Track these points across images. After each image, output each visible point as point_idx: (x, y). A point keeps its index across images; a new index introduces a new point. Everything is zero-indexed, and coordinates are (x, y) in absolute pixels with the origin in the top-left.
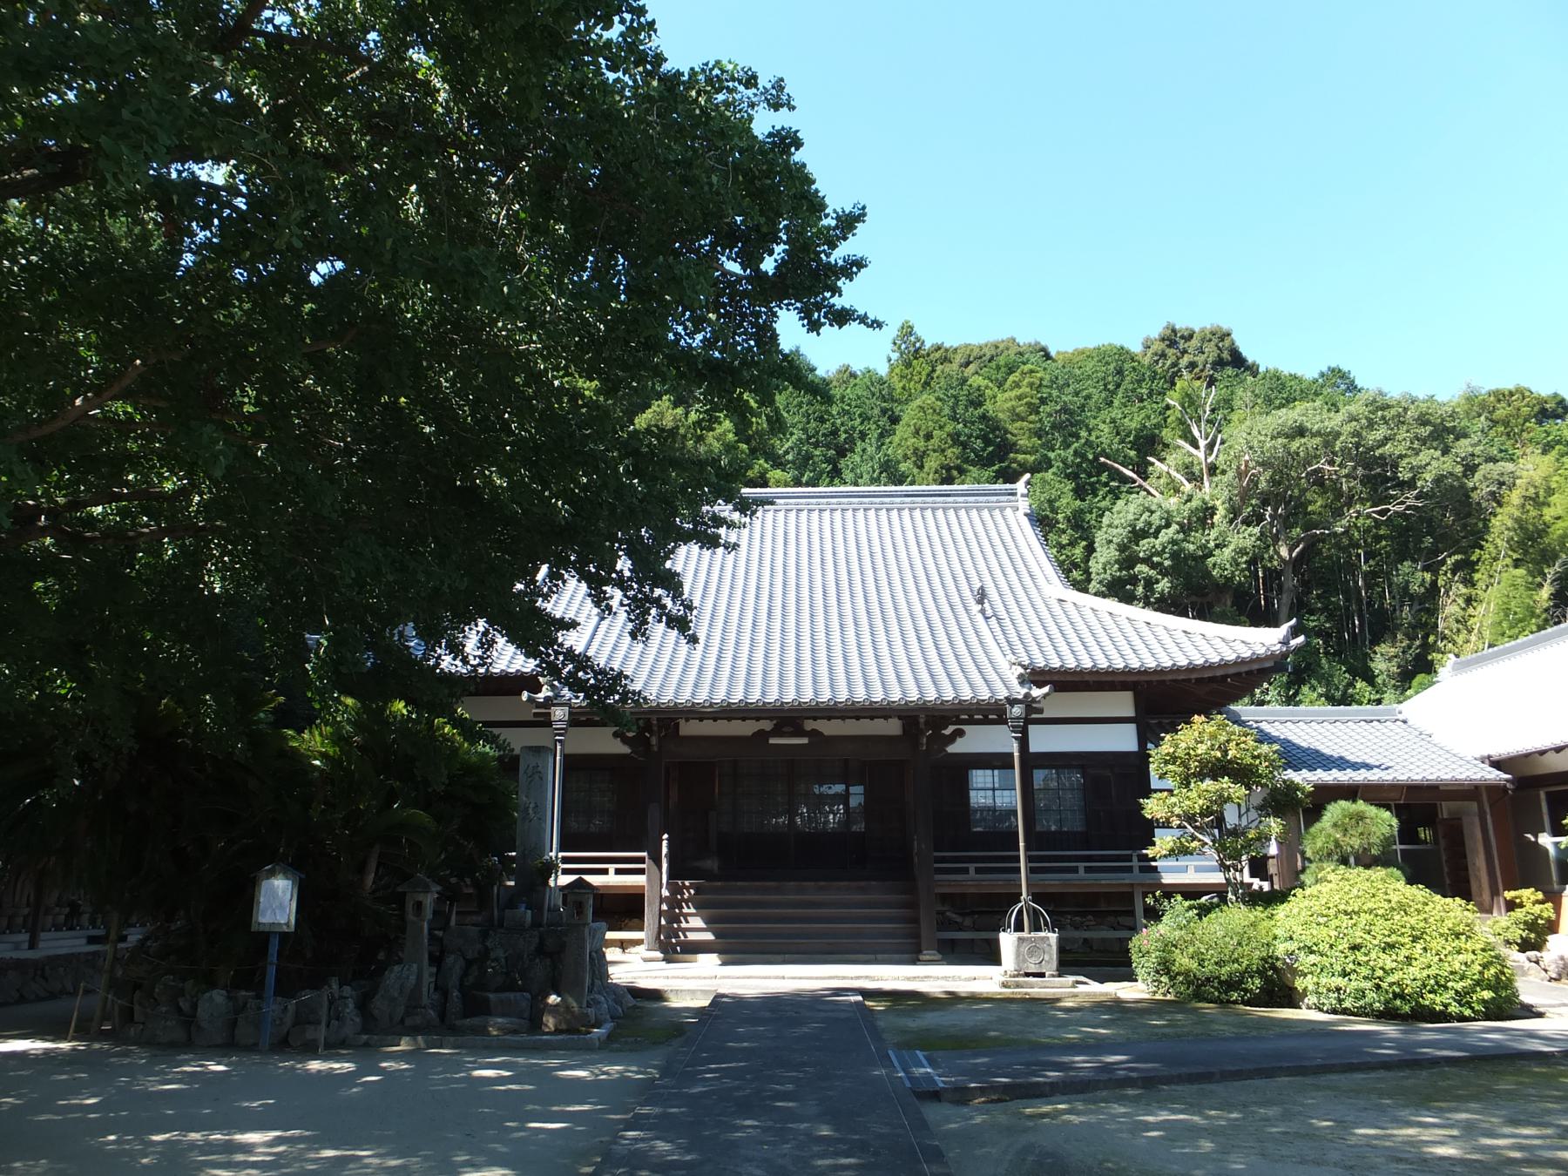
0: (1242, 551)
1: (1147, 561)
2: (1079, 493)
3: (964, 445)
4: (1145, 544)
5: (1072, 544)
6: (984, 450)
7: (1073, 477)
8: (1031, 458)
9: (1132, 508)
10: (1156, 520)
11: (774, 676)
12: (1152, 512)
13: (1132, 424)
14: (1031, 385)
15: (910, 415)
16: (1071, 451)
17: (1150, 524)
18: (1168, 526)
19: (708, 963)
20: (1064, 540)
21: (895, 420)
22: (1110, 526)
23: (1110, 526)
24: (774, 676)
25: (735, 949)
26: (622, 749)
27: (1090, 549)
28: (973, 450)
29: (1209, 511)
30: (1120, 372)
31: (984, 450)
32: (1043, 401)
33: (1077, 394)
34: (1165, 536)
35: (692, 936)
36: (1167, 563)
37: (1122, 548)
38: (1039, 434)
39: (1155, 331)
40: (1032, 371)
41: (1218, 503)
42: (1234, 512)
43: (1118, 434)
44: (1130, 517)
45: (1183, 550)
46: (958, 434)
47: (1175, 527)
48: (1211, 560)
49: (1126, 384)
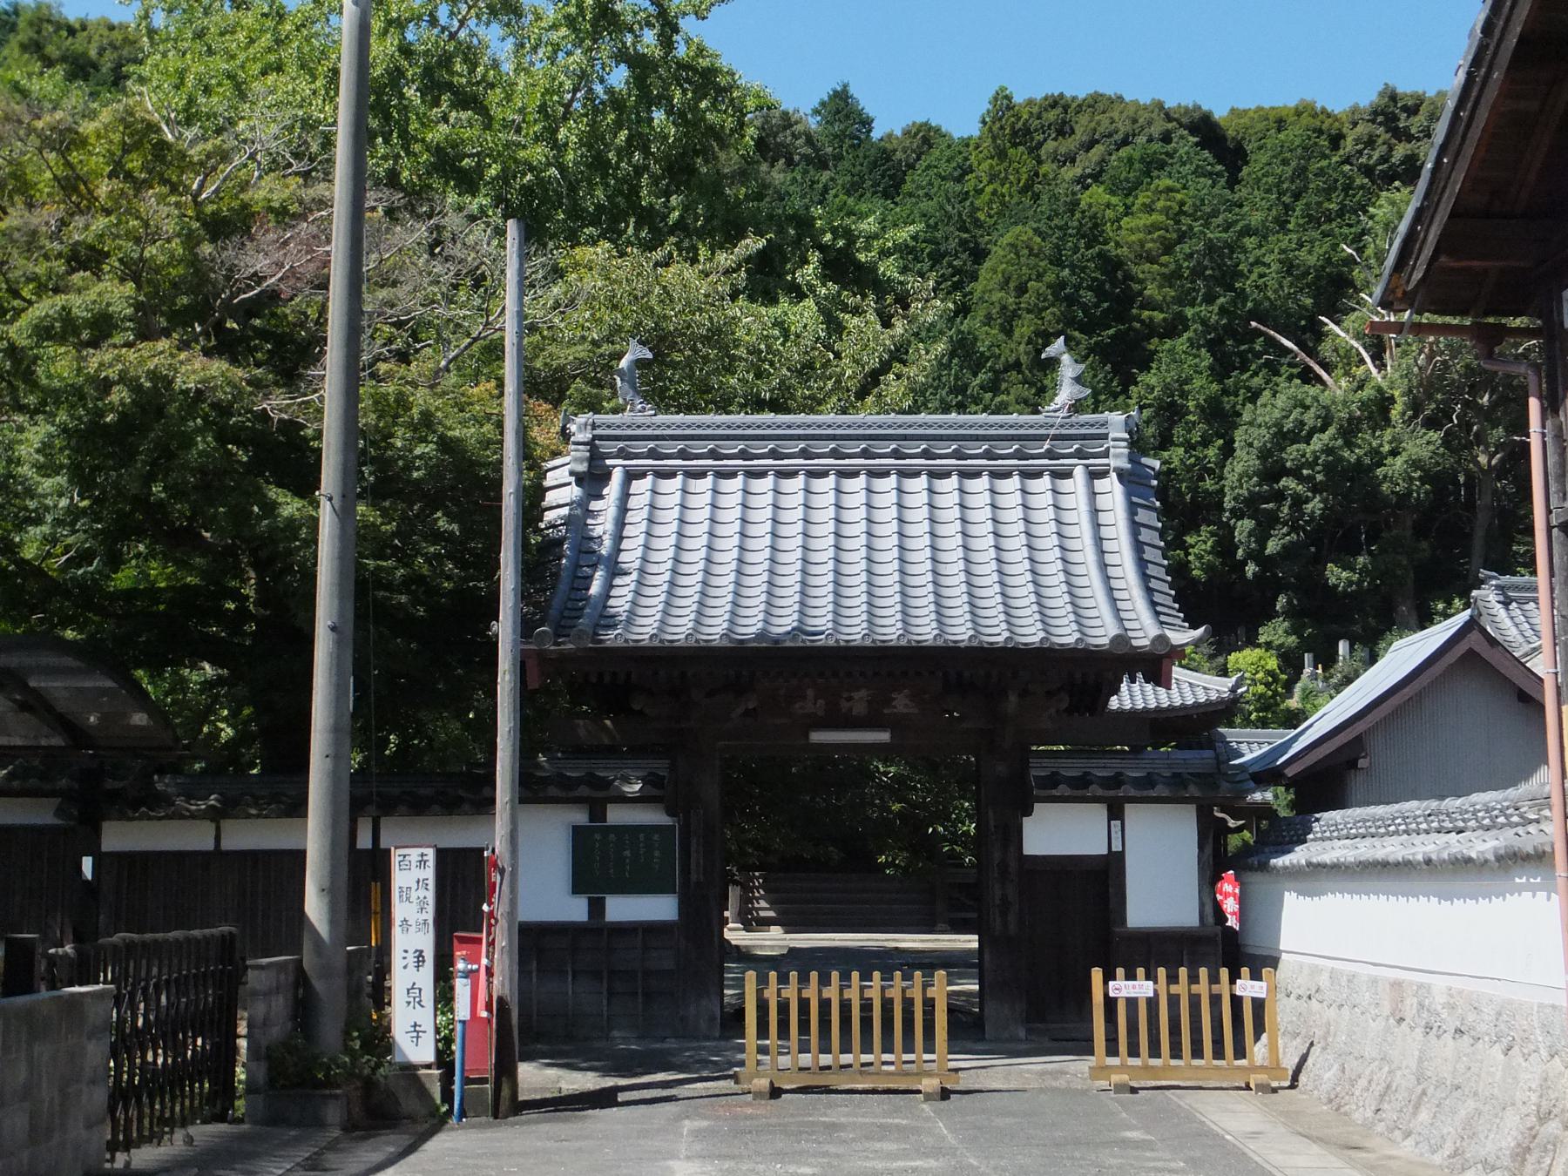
0: (1415, 464)
1: (1295, 473)
2: (1221, 370)
3: (1071, 300)
4: (1292, 453)
5: (1205, 442)
6: (1097, 306)
7: (1212, 346)
8: (1159, 316)
9: (1281, 401)
10: (1310, 418)
11: (757, 582)
12: (1307, 408)
13: (1310, 258)
14: (1166, 211)
15: (1003, 242)
16: (1216, 309)
17: (1302, 423)
18: (1323, 430)
19: (776, 931)
20: (1196, 437)
21: (979, 255)
22: (1251, 424)
23: (1251, 424)
24: (757, 582)
25: (792, 924)
26: (1273, 861)
27: (1228, 451)
28: (1085, 308)
29: (1383, 403)
30: (1301, 172)
31: (1097, 306)
32: (1182, 237)
33: (1227, 227)
34: (1318, 441)
35: (762, 914)
36: (1319, 477)
37: (1264, 454)
38: (1170, 279)
39: (1367, 97)
40: (1170, 190)
41: (1397, 393)
42: (1415, 406)
43: (1289, 273)
44: (1277, 414)
45: (1342, 459)
46: (1062, 285)
47: (1332, 430)
48: (1380, 471)
49: (1310, 198)
